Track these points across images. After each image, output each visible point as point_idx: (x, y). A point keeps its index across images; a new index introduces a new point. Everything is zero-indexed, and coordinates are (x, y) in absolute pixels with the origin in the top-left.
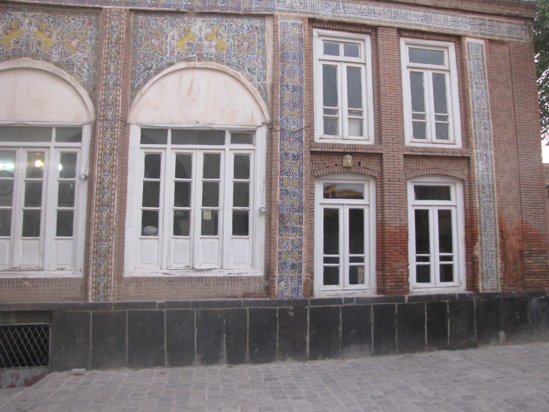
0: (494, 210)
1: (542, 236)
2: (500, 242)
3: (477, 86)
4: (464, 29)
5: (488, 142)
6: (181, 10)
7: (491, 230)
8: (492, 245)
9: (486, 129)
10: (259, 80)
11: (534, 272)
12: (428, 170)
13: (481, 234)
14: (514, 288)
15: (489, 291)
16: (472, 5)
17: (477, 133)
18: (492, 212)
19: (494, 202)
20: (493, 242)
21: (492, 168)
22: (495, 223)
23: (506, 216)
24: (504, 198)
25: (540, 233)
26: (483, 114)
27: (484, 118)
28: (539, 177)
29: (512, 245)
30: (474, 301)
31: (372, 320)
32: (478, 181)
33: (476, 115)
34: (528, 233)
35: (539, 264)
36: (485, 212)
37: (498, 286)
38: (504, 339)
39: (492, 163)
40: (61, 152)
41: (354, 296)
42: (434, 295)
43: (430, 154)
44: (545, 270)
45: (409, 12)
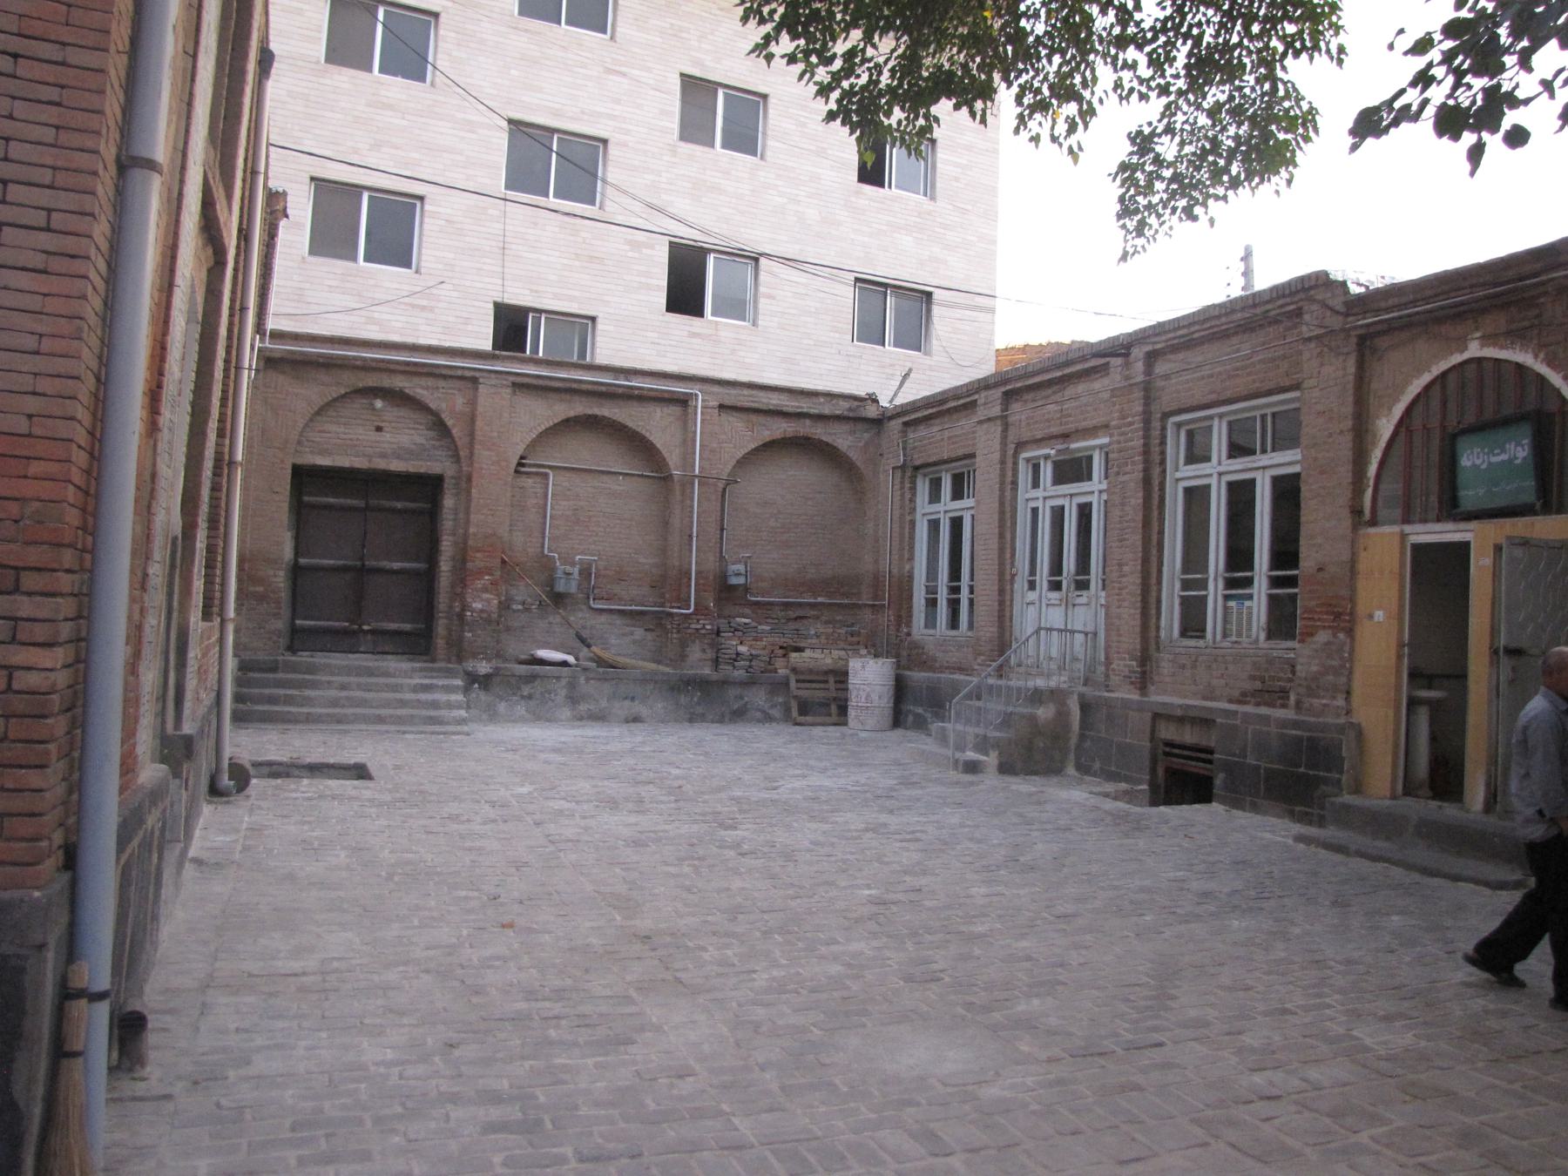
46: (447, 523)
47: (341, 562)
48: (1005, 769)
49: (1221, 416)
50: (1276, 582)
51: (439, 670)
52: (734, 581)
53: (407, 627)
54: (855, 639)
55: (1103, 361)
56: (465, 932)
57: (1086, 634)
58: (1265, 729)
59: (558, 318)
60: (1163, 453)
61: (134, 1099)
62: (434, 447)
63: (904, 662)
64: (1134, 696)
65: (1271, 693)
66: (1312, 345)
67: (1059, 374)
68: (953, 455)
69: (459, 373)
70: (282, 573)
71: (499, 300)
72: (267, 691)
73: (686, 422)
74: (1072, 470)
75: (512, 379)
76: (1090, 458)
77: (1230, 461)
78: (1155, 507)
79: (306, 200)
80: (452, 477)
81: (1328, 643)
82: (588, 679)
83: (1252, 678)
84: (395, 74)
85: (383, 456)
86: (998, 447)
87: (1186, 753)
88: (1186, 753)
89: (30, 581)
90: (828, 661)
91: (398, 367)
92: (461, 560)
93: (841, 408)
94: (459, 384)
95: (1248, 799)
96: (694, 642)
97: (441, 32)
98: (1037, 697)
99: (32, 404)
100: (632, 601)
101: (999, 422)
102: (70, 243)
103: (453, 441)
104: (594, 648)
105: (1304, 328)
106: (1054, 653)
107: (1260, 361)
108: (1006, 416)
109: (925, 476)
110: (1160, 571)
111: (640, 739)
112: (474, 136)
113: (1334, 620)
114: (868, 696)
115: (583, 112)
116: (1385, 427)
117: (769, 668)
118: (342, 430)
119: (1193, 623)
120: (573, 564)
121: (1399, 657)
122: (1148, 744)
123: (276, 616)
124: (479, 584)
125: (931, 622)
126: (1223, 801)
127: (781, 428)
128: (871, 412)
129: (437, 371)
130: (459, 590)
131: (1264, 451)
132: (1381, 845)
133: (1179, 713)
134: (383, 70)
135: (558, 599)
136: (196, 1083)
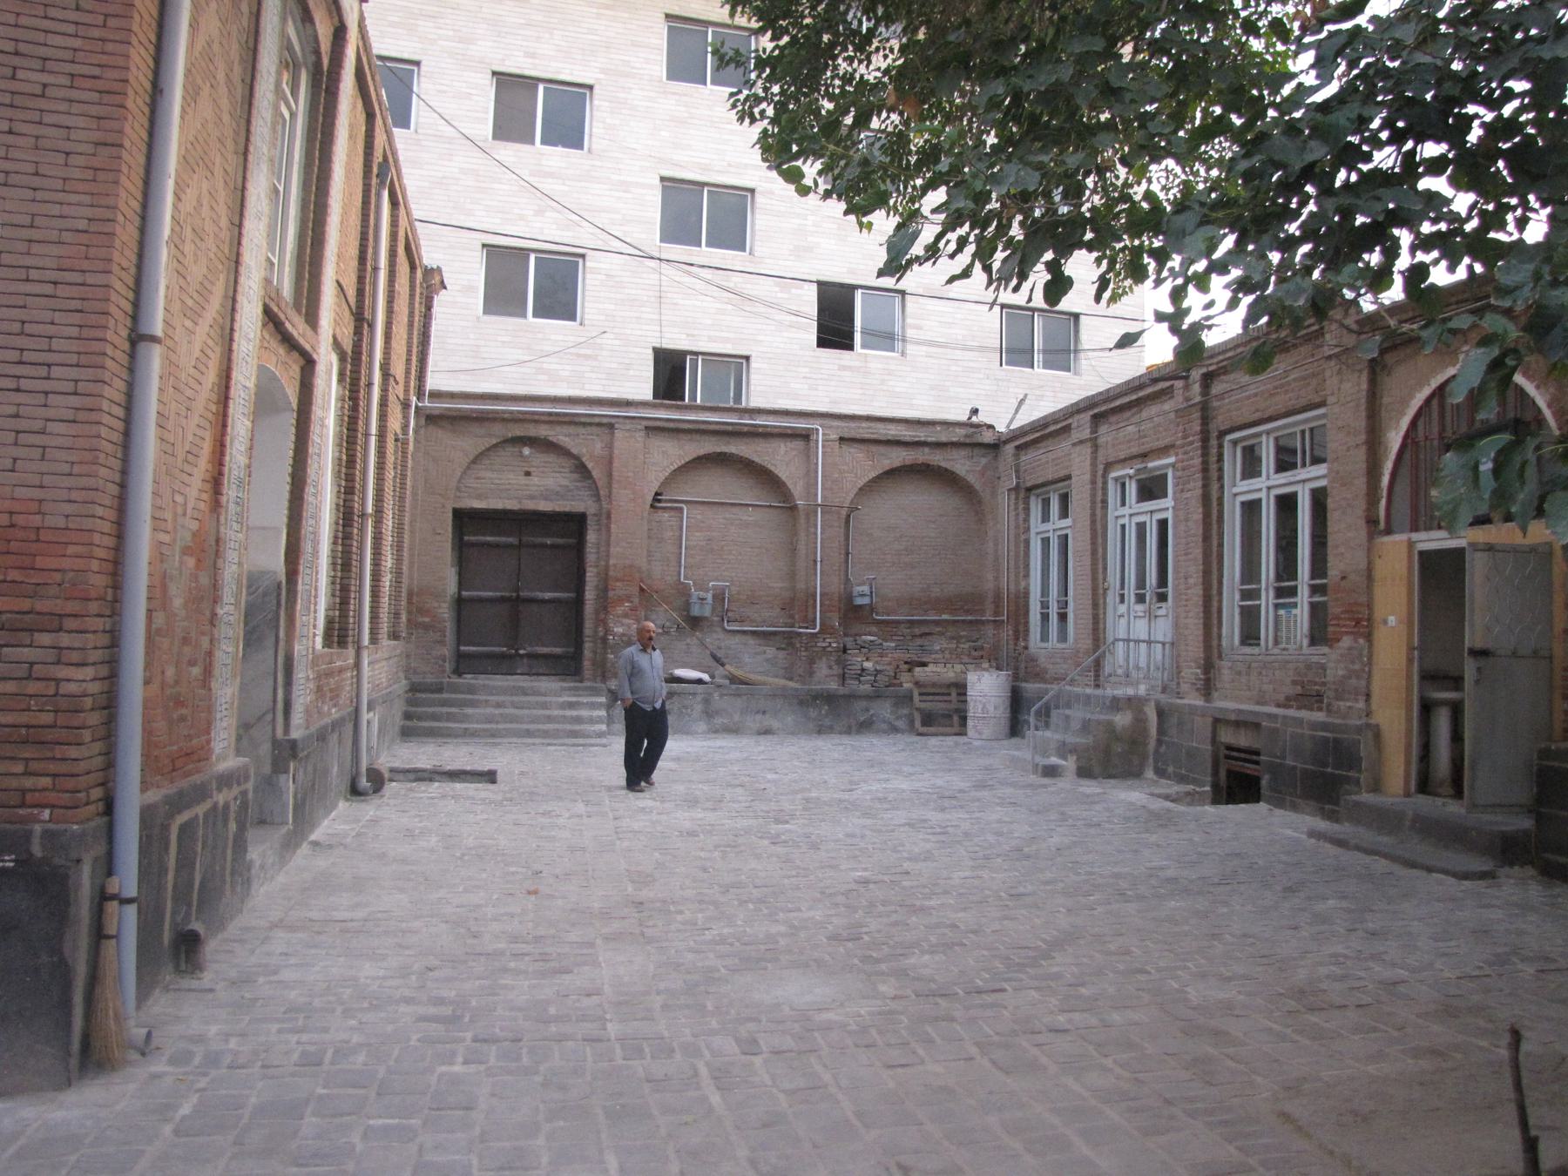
28: (82, 225)
42: (1452, 751)
44: (47, 718)
46: (591, 556)
47: (498, 594)
48: (1084, 772)
49: (1268, 433)
50: (1315, 590)
51: (586, 689)
52: (859, 601)
53: (558, 650)
54: (981, 653)
55: (1167, 384)
56: (495, 897)
57: (1164, 644)
58: (1299, 731)
59: (716, 360)
60: (1221, 470)
61: (190, 990)
62: (578, 488)
63: (1022, 674)
64: (1199, 702)
65: (1309, 697)
66: (1333, 363)
67: (1134, 397)
68: (1056, 476)
69: (597, 420)
70: (445, 605)
71: (658, 345)
73: (808, 455)
74: (1151, 489)
75: (645, 423)
76: (1165, 476)
77: (1277, 476)
78: (1214, 522)
79: (478, 266)
80: (595, 515)
81: (1350, 649)
82: (722, 695)
83: (1294, 683)
84: (555, 145)
85: (532, 497)
86: (1088, 468)
87: (1243, 755)
88: (1243, 755)
89: (70, 624)
90: (951, 674)
91: (543, 418)
92: (603, 590)
93: (958, 435)
94: (595, 429)
95: (1288, 798)
96: (820, 658)
97: (596, 102)
98: (1116, 704)
99: (69, 508)
100: (764, 623)
101: (1089, 444)
102: (88, 402)
103: (594, 482)
104: (727, 667)
105: (1326, 348)
106: (1143, 664)
107: (1294, 380)
108: (1096, 438)
109: (1038, 496)
110: (1220, 583)
111: (762, 748)
112: (629, 196)
113: (1355, 626)
114: (984, 707)
115: (730, 165)
116: (1394, 440)
117: (894, 681)
118: (495, 475)
119: (1250, 635)
120: (707, 590)
121: (1410, 661)
122: (1210, 748)
123: (442, 643)
124: (620, 610)
125: (1045, 637)
126: (1268, 802)
127: (898, 457)
128: (987, 437)
129: (576, 419)
130: (602, 616)
131: (1304, 465)
132: (1385, 840)
133: (1233, 717)
134: (544, 142)
135: (695, 622)
136: (234, 983)
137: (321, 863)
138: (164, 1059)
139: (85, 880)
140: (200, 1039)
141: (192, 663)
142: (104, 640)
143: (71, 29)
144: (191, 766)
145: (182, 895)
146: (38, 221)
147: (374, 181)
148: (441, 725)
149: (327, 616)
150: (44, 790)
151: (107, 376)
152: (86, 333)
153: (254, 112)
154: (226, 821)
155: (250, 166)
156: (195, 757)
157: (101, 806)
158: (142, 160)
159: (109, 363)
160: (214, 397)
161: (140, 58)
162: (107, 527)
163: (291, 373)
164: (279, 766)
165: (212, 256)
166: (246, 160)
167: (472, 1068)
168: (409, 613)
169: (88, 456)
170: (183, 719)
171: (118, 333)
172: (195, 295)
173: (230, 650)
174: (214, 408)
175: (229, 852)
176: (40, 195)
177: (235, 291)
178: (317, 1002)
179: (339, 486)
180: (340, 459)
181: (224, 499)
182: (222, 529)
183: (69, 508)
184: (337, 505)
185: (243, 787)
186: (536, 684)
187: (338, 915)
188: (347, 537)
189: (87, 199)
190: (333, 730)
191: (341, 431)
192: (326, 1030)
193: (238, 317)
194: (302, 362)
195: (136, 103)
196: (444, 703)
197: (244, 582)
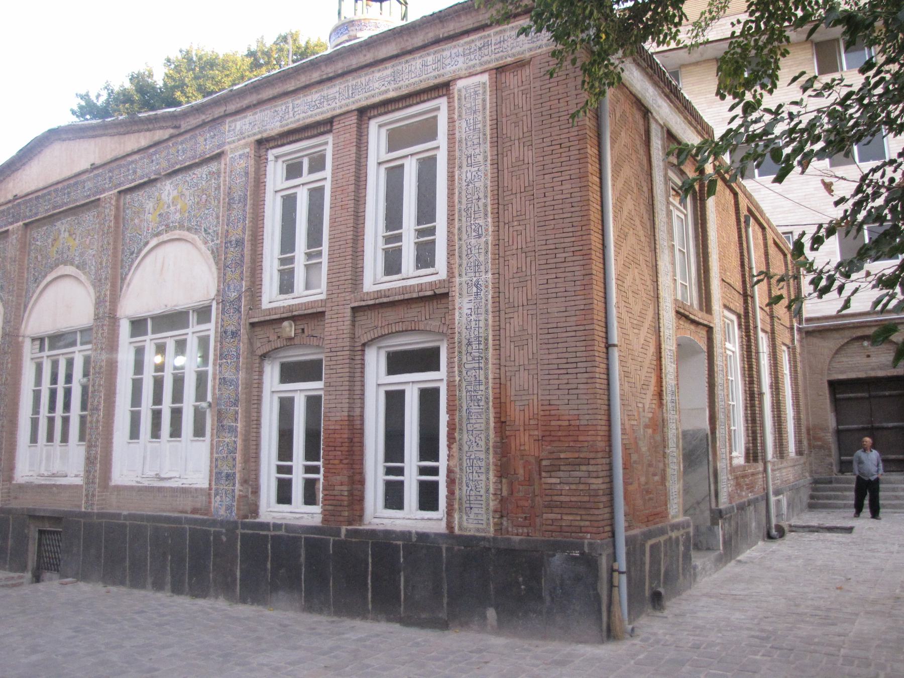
0: (487, 383)
1: (581, 428)
2: (495, 442)
3: (469, 162)
4: (454, 67)
5: (482, 259)
6: (152, 178)
7: (479, 421)
8: (479, 449)
9: (479, 236)
10: (213, 241)
11: (561, 502)
12: (390, 326)
13: (460, 429)
14: (525, 530)
15: (472, 533)
16: (459, 22)
17: (464, 248)
18: (482, 387)
19: (487, 369)
20: (482, 443)
21: (486, 305)
22: (488, 408)
23: (513, 393)
24: (512, 359)
25: (577, 423)
26: (476, 209)
27: (477, 216)
28: (582, 307)
29: (522, 448)
30: (444, 547)
31: (302, 559)
32: (459, 333)
33: (464, 214)
34: (553, 423)
35: (573, 487)
36: (469, 388)
37: (488, 524)
38: (495, 623)
39: (486, 296)
40: (135, 347)
41: (284, 522)
43: (385, 300)
44: (586, 499)
45: (371, 76)
47: (861, 426)
72: (825, 493)
85: (873, 369)
89: (592, 462)
91: (872, 324)
99: (588, 417)
123: (830, 456)
137: (738, 570)
138: (640, 639)
139: (604, 562)
140: (655, 634)
141: (654, 475)
142: (607, 467)
143: (571, 234)
144: (657, 520)
145: (655, 575)
146: (568, 309)
147: (743, 225)
148: (830, 502)
149: (746, 447)
150: (587, 526)
151: (596, 364)
152: (588, 348)
153: (657, 231)
154: (678, 545)
155: (658, 255)
156: (660, 516)
157: (610, 534)
158: (602, 275)
159: (597, 359)
160: (655, 358)
161: (595, 238)
162: (603, 423)
163: (700, 335)
164: (714, 522)
165: (644, 299)
166: (655, 253)
167: (765, 658)
168: (809, 440)
169: (592, 396)
170: (651, 499)
171: (600, 346)
172: (638, 318)
173: (676, 468)
174: (655, 363)
175: (681, 559)
176: (568, 299)
177: (658, 310)
178: (708, 626)
179: (745, 381)
180: (744, 367)
181: (665, 402)
182: (665, 415)
183: (588, 417)
184: (745, 390)
185: (687, 530)
186: (888, 477)
187: (734, 592)
188: (753, 406)
189: (582, 297)
190: (749, 505)
191: (743, 354)
192: (707, 636)
193: (661, 321)
194: (706, 329)
195: (596, 256)
196: (833, 490)
197: (680, 436)
